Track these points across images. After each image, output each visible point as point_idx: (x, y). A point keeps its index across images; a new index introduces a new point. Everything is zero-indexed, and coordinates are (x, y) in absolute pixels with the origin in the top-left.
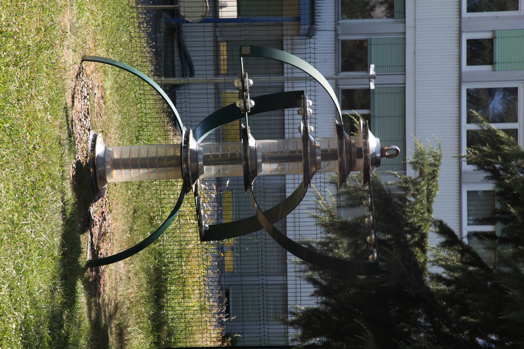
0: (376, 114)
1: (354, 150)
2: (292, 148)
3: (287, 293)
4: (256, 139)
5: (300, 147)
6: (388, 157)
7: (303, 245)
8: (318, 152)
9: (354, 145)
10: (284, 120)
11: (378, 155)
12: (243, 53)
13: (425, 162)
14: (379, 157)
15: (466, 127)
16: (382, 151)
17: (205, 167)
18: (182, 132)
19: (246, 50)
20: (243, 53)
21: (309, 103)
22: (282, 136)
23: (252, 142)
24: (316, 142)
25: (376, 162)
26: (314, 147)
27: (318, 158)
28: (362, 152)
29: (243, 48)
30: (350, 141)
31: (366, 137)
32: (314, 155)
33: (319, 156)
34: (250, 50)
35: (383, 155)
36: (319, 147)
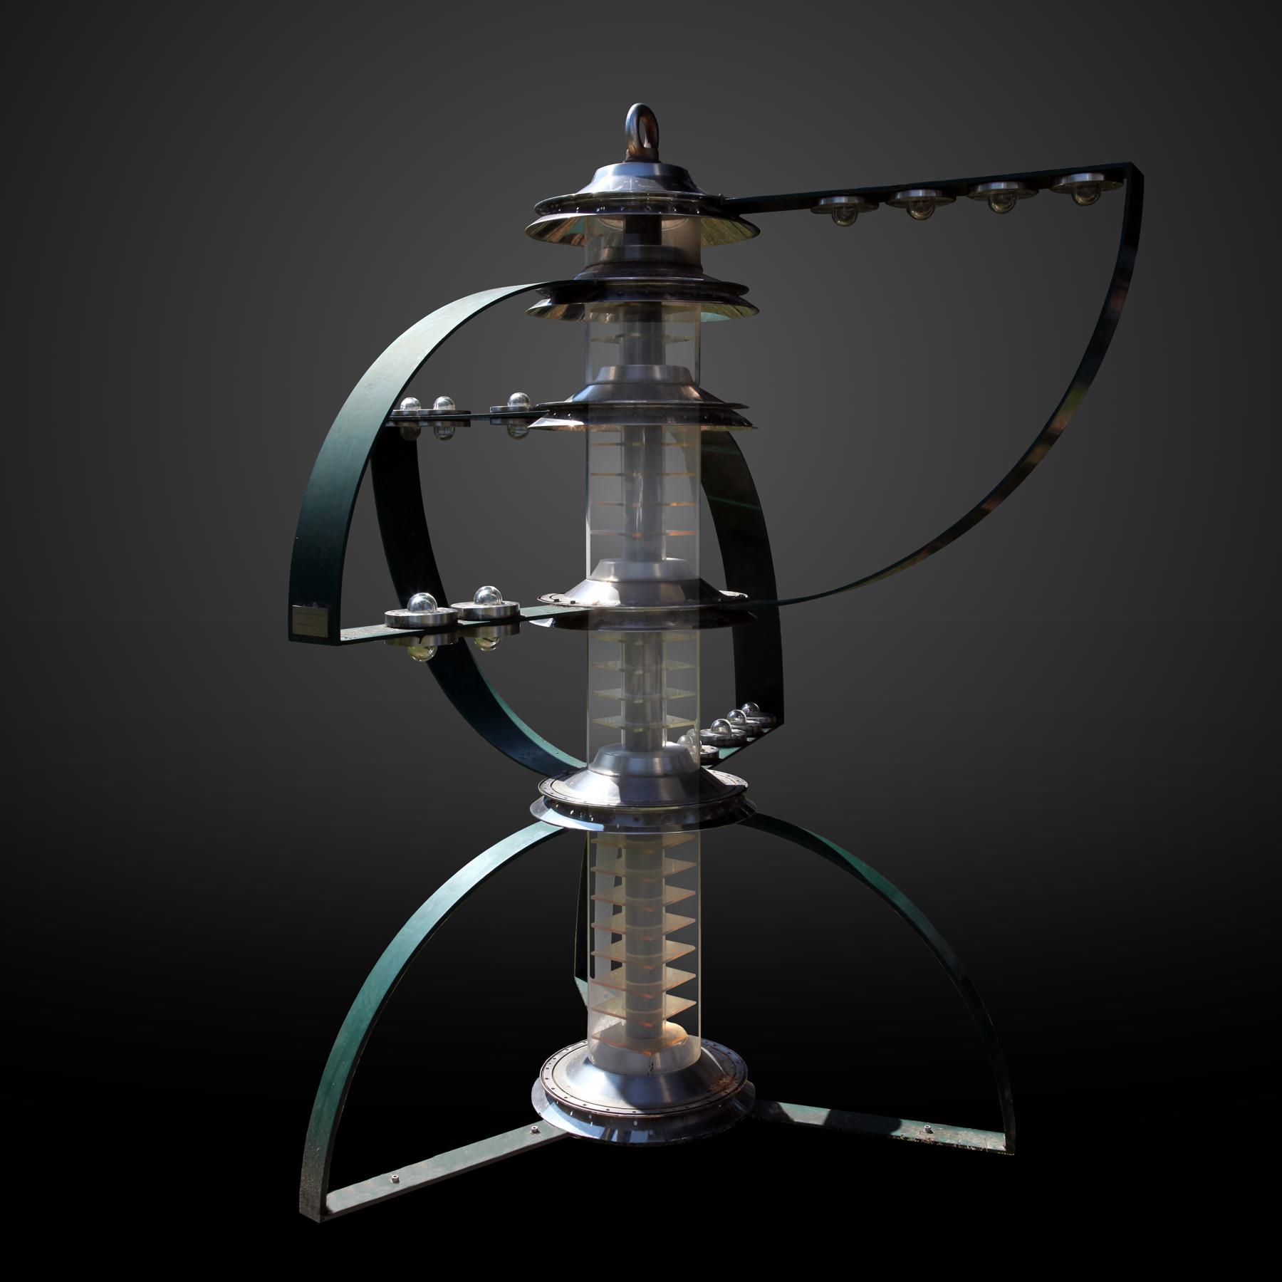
6: (654, 143)
7: (720, 776)
8: (636, 372)
9: (619, 250)
13: (622, 753)
16: (641, 157)
19: (312, 618)
20: (323, 632)
23: (598, 592)
24: (601, 378)
25: (677, 178)
26: (620, 386)
27: (657, 373)
28: (640, 219)
29: (298, 630)
30: (605, 263)
31: (588, 204)
32: (648, 388)
33: (652, 370)
36: (622, 372)
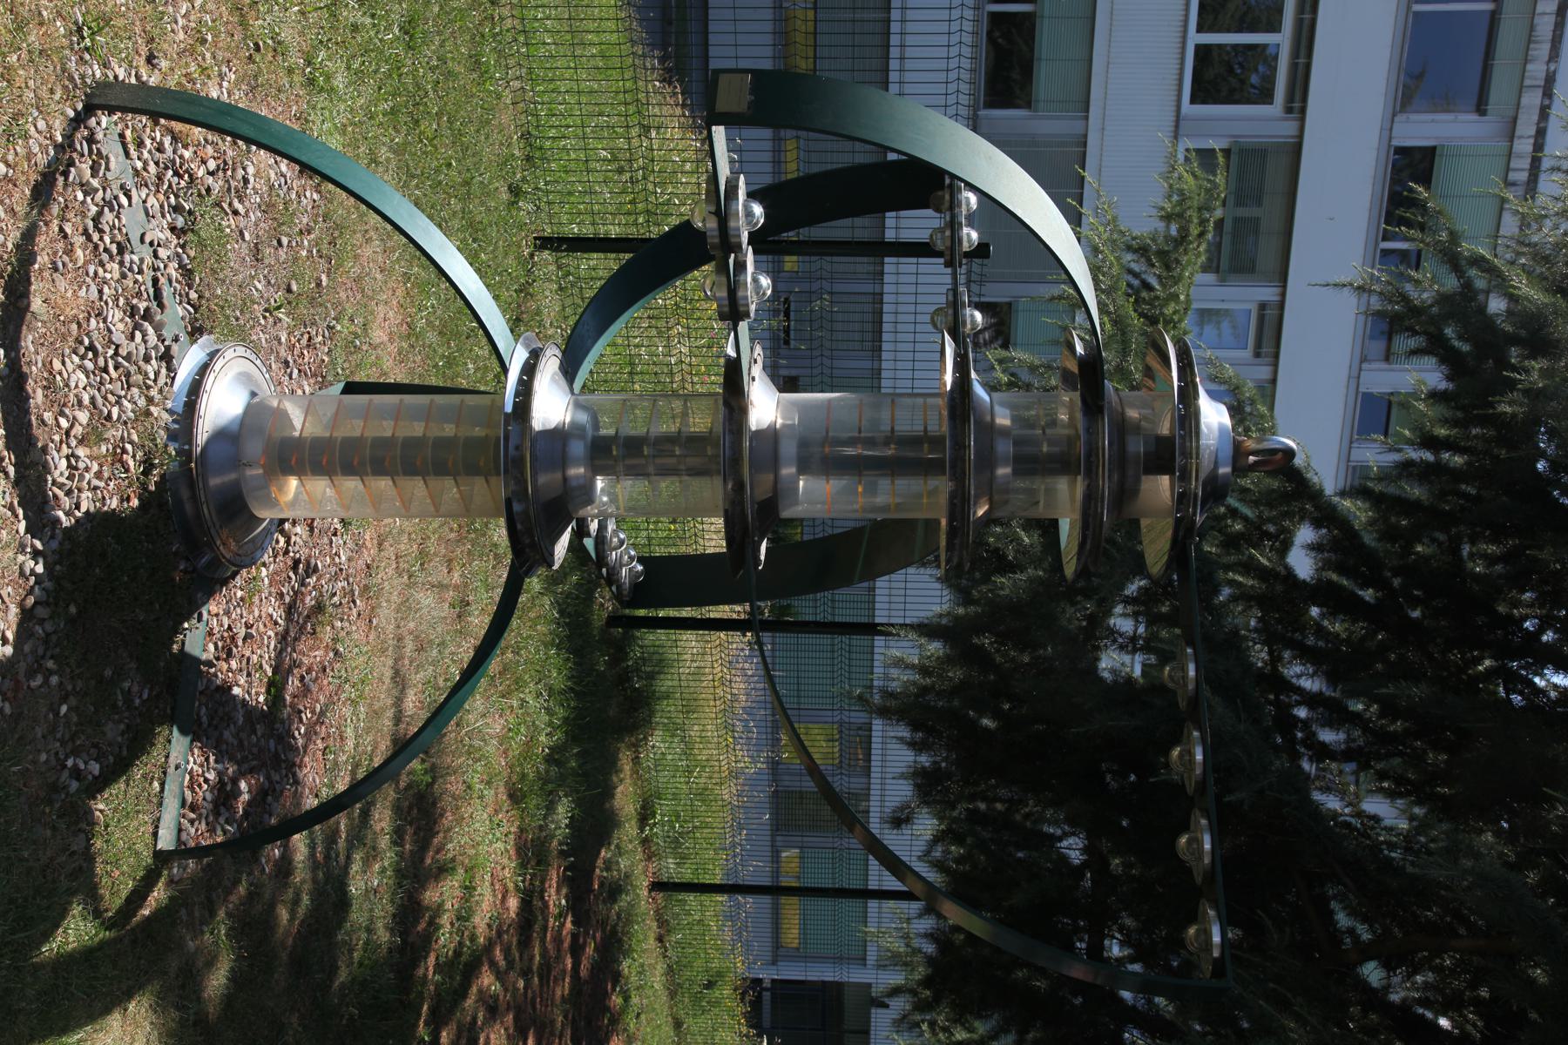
0: (1046, 13)
1: (1136, 446)
2: (908, 422)
3: (881, 313)
4: (786, 383)
5: (939, 424)
9: (1137, 428)
10: (888, 21)
11: (1225, 470)
12: (722, 106)
14: (1225, 475)
15: (1195, 38)
17: (600, 483)
18: (505, 370)
21: (968, 203)
22: (871, 381)
24: (997, 409)
26: (988, 430)
30: (1123, 413)
34: (753, 91)
35: (1240, 468)
